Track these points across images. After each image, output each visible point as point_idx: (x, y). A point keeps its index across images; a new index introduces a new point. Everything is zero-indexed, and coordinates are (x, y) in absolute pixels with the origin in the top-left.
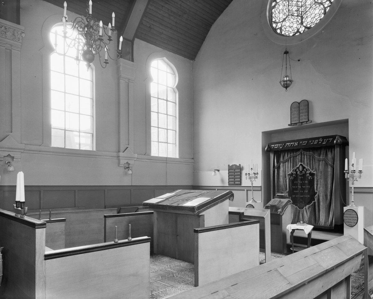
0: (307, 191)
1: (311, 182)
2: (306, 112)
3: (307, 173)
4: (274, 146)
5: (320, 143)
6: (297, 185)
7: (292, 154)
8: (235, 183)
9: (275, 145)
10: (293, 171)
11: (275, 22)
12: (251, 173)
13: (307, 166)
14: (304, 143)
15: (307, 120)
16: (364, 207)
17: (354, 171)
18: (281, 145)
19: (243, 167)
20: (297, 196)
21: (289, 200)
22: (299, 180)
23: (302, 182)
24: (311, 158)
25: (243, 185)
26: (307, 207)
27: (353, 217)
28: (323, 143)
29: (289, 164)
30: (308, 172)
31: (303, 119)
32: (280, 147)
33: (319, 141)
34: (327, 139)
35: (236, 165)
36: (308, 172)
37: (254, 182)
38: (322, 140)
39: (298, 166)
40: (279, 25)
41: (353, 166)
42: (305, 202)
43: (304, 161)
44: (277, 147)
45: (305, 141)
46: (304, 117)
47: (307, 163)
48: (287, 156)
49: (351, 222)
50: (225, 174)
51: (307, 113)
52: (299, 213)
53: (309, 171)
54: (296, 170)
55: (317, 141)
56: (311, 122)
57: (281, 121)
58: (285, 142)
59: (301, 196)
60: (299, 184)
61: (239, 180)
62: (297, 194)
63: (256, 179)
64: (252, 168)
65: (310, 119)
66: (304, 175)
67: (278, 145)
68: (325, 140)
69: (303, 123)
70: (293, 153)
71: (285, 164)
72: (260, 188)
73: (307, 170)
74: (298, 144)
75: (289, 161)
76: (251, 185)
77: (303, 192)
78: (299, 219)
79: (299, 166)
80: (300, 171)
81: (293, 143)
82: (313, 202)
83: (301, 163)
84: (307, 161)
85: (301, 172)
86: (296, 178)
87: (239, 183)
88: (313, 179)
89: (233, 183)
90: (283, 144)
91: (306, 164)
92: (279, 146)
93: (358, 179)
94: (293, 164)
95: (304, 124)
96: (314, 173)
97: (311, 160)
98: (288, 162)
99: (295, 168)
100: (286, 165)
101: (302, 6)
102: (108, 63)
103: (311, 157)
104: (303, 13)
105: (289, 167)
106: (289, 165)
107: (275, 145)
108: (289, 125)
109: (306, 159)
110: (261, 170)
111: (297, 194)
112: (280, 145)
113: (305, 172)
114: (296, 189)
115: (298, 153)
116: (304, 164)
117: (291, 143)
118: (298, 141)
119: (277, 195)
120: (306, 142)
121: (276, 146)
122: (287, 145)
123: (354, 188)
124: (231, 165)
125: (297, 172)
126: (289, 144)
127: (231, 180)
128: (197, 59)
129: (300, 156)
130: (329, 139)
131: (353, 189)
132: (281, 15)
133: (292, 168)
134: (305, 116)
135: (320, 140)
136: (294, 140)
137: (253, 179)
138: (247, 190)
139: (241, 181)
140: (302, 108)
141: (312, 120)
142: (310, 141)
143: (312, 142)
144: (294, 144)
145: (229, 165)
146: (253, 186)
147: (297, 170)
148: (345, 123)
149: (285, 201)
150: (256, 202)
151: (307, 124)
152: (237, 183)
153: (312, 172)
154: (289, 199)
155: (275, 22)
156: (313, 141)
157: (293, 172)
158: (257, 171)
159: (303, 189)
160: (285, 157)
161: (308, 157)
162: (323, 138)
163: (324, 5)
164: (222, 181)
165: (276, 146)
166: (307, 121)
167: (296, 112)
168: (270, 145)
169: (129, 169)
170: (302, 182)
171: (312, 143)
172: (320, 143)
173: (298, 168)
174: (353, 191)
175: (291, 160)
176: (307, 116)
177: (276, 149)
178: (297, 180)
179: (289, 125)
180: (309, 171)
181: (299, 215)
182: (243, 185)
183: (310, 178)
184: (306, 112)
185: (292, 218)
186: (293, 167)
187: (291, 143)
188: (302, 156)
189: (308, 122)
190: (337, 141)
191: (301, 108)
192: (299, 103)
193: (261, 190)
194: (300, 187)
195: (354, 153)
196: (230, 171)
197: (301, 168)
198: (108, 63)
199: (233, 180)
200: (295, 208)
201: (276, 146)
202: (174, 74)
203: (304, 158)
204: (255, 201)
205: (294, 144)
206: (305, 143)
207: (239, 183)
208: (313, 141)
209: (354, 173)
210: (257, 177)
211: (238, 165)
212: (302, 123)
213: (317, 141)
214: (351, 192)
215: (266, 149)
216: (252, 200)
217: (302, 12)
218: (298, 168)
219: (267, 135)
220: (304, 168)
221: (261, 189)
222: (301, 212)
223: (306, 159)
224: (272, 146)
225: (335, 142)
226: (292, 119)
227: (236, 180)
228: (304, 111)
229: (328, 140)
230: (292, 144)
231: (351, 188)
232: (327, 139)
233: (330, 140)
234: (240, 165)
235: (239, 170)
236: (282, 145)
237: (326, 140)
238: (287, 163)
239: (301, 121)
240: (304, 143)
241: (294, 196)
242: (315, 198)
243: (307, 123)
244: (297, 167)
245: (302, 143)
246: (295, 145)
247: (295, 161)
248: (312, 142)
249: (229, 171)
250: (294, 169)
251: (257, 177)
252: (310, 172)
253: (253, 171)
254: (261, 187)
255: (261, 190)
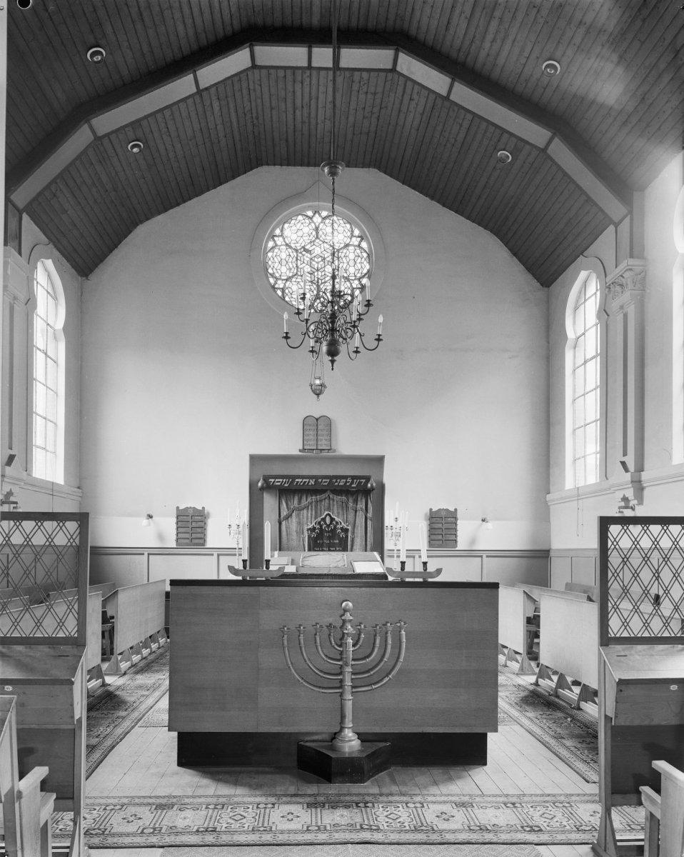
4: (274, 482)
5: (348, 484)
11: (272, 275)
12: (394, 527)
19: (208, 513)
30: (339, 526)
31: (323, 444)
33: (346, 482)
38: (350, 481)
40: (280, 284)
44: (279, 484)
45: (306, 478)
47: (338, 513)
50: (169, 526)
54: (319, 523)
55: (345, 480)
57: (284, 440)
67: (281, 480)
68: (355, 481)
73: (337, 523)
76: (235, 546)
81: (307, 480)
85: (328, 526)
94: (316, 512)
95: (324, 454)
99: (319, 519)
101: (318, 270)
102: (359, 352)
104: (320, 281)
105: (310, 517)
108: (300, 451)
113: (335, 527)
115: (323, 496)
118: (316, 477)
120: (328, 480)
122: (298, 482)
124: (182, 507)
125: (321, 526)
126: (300, 480)
128: (92, 277)
132: (284, 269)
138: (218, 555)
140: (317, 427)
144: (309, 482)
145: (178, 508)
148: (380, 460)
151: (328, 454)
155: (272, 275)
156: (338, 481)
162: (353, 478)
163: (351, 284)
164: (161, 537)
165: (278, 482)
167: (311, 433)
169: (15, 505)
171: (336, 484)
172: (348, 484)
173: (324, 520)
175: (312, 506)
179: (300, 451)
182: (208, 546)
186: (316, 518)
191: (320, 427)
192: (317, 420)
198: (359, 352)
202: (55, 298)
205: (309, 482)
212: (321, 450)
217: (318, 279)
218: (324, 520)
219: (255, 460)
220: (332, 519)
234: (203, 508)
239: (320, 448)
249: (177, 519)
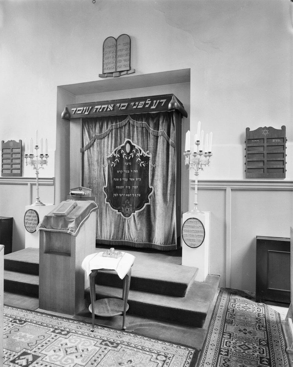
0: (136, 187)
1: (144, 172)
2: (127, 55)
3: (138, 157)
5: (147, 106)
6: (121, 176)
7: (114, 124)
8: (13, 172)
9: (78, 109)
10: (115, 152)
12: (35, 155)
13: (138, 145)
14: (123, 106)
15: (128, 69)
16: (211, 212)
17: (210, 153)
18: (87, 108)
20: (121, 195)
21: (92, 204)
22: (125, 168)
23: (130, 171)
24: (144, 131)
25: (25, 176)
26: (136, 213)
27: (198, 232)
28: (152, 107)
29: (110, 141)
32: (85, 112)
33: (145, 104)
34: (158, 101)
35: (14, 142)
36: (138, 155)
37: (40, 171)
38: (150, 102)
39: (123, 145)
41: (198, 145)
42: (133, 206)
43: (133, 137)
44: (80, 112)
46: (123, 63)
48: (106, 127)
49: (194, 240)
51: (128, 57)
52: (124, 223)
53: (141, 153)
54: (120, 151)
55: (143, 103)
56: (134, 72)
57: (87, 69)
58: (93, 104)
59: (127, 195)
60: (124, 175)
61: (19, 166)
62: (120, 191)
63: (44, 166)
64: (37, 146)
65: (133, 67)
66: (132, 160)
67: (82, 108)
68: (155, 101)
69: (122, 73)
70: (116, 122)
71: (103, 140)
72: (52, 180)
73: (137, 151)
74: (113, 107)
75: (110, 135)
76: (35, 176)
77: (131, 187)
78: (124, 233)
79: (126, 144)
80: (126, 153)
81: (106, 106)
82: (146, 204)
83: (129, 140)
84: (137, 136)
85: (128, 154)
86: (120, 165)
87: (19, 172)
88: (147, 166)
89: (9, 172)
90: (90, 108)
91: (136, 141)
92: (83, 110)
93: (203, 166)
96: (148, 156)
97: (148, 136)
98: (108, 137)
99: (119, 147)
100: (104, 142)
103: (144, 129)
105: (110, 146)
106: (110, 143)
107: (122, 105)
108: (100, 76)
109: (135, 133)
110: (55, 149)
111: (120, 191)
112: (85, 108)
113: (135, 155)
114: (120, 183)
115: (124, 122)
116: (133, 140)
117: (103, 106)
118: (114, 102)
119: (72, 194)
120: (126, 104)
121: (79, 110)
122: (97, 109)
123: (198, 181)
125: (121, 155)
127: (5, 166)
129: (127, 127)
130: (161, 101)
131: (196, 183)
133: (113, 147)
134: (125, 60)
135: (147, 102)
136: (108, 101)
137: (39, 166)
139: (21, 169)
141: (136, 69)
142: (132, 104)
143: (135, 105)
144: (108, 107)
146: (39, 177)
147: (122, 151)
149: (84, 205)
150: (44, 205)
152: (15, 172)
153: (146, 154)
154: (92, 202)
156: (137, 103)
157: (114, 155)
158: (47, 151)
159: (130, 183)
160: (103, 129)
161: (140, 129)
162: (153, 98)
166: (128, 71)
167: (111, 55)
168: (69, 108)
170: (130, 171)
171: (135, 107)
172: (147, 106)
173: (124, 148)
174: (196, 187)
176: (129, 62)
177: (82, 114)
178: (122, 169)
180: (141, 153)
181: (123, 227)
183: (142, 165)
184: (127, 55)
185: (113, 232)
187: (103, 106)
188: (129, 128)
189: (129, 72)
190: (173, 104)
191: (119, 47)
192: (116, 40)
193: (54, 185)
194: (125, 180)
195: (200, 123)
196: (5, 151)
197: (128, 148)
199: (9, 166)
200: (118, 216)
201: (79, 110)
203: (133, 132)
204: (41, 203)
206: (124, 106)
207: (19, 172)
208: (137, 103)
209: (210, 156)
210: (45, 162)
211: (18, 141)
213: (143, 103)
214: (194, 189)
215: (62, 114)
216: (37, 202)
218: (124, 148)
219: (66, 91)
220: (132, 147)
221: (54, 182)
222: (126, 221)
223: (135, 133)
224: (72, 109)
225: (170, 105)
226: (105, 66)
227: (14, 166)
228: (124, 52)
229: (159, 102)
230: (104, 108)
231: (194, 181)
232: (158, 101)
233: (163, 102)
234: (21, 141)
235: (19, 150)
236: (89, 108)
237: (156, 103)
238: (106, 139)
239: (119, 70)
240: (123, 106)
241: (116, 195)
242: (149, 199)
243: (127, 74)
244: (122, 145)
245: (120, 106)
246: (109, 110)
247: (119, 135)
248: (135, 105)
250: (116, 149)
251: (45, 162)
252: (141, 154)
253: (39, 152)
254: (53, 179)
255: (54, 185)
